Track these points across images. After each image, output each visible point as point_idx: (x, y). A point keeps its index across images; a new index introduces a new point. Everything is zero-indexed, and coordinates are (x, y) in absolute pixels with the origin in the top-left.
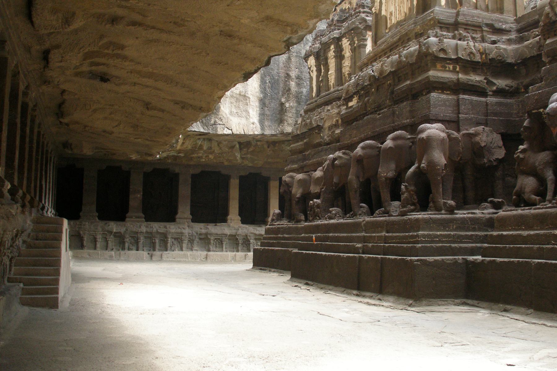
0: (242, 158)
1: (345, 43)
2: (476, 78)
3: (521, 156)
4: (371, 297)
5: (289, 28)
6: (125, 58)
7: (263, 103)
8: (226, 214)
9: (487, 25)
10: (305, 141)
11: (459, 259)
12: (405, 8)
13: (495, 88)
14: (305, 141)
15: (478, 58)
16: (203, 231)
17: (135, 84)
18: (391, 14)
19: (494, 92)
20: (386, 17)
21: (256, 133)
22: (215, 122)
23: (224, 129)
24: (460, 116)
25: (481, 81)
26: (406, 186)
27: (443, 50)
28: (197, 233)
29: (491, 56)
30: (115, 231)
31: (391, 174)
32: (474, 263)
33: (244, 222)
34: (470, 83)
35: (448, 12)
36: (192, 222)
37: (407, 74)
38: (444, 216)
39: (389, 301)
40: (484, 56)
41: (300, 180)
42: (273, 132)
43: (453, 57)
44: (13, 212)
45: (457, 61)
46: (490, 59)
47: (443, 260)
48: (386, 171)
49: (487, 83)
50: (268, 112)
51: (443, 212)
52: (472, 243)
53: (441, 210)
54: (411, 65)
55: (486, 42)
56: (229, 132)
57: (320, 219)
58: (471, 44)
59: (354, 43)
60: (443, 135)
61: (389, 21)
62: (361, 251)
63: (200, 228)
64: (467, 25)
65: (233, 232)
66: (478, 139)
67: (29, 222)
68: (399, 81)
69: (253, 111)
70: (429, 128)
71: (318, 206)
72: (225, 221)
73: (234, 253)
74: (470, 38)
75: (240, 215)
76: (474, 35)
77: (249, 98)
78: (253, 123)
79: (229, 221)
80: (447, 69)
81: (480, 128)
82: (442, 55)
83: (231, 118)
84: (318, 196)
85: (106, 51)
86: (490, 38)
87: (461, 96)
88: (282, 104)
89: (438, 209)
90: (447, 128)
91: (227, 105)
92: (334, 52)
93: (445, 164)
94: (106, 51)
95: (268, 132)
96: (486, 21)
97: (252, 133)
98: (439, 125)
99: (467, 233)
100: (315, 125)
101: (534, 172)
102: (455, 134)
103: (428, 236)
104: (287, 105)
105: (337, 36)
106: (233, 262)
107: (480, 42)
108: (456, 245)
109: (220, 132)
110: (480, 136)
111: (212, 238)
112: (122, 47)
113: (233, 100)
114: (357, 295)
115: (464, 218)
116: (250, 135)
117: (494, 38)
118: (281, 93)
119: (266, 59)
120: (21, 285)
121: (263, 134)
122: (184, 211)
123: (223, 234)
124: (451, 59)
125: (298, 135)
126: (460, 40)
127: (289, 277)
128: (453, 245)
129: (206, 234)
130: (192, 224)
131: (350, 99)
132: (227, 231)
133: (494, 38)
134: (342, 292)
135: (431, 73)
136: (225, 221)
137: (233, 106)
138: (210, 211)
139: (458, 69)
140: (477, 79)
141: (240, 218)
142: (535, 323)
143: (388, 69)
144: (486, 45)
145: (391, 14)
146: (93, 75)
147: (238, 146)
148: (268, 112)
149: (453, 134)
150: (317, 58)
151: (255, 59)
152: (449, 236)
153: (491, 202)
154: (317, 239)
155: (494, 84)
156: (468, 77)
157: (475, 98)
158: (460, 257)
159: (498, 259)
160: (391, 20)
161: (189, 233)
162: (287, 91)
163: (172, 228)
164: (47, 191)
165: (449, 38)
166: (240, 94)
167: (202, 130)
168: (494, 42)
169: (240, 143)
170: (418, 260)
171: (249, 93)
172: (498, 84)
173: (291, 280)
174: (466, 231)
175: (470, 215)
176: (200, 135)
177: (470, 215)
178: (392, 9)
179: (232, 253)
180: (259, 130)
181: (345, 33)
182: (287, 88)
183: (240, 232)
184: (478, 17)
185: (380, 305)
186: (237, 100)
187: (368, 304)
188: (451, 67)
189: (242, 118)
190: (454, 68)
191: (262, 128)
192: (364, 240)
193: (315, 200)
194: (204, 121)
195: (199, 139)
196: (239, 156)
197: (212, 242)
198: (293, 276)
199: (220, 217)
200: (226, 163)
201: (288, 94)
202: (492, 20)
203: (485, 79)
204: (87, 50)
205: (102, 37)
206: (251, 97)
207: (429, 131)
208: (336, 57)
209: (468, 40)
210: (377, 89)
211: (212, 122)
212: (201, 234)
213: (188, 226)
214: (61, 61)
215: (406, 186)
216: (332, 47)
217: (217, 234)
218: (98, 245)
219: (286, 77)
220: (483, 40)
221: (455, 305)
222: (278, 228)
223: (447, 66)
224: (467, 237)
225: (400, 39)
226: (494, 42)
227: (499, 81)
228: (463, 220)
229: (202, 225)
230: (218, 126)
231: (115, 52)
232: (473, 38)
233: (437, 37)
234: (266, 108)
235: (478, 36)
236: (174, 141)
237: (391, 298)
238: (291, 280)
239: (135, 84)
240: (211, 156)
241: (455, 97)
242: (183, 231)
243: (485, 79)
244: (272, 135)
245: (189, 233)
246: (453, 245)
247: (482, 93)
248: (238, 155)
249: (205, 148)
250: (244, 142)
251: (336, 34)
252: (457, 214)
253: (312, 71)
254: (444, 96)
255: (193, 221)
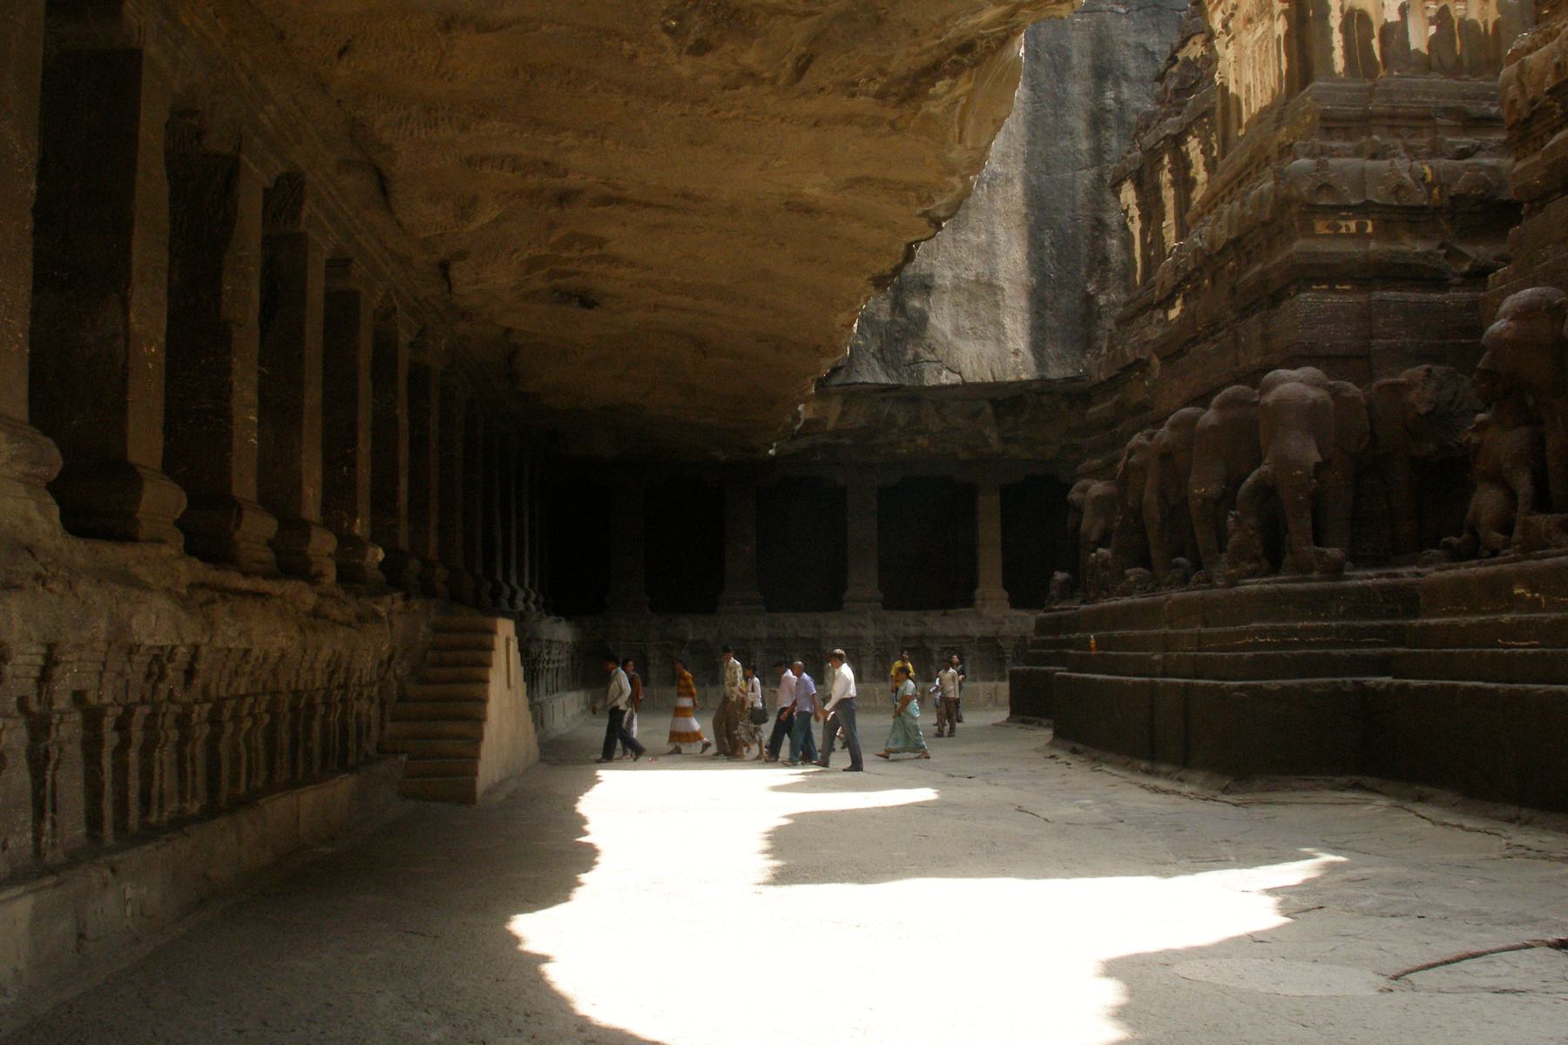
0: (1005, 440)
1: (1193, 146)
2: (1414, 246)
3: (1475, 439)
4: (1168, 776)
5: (911, 194)
6: (615, 260)
7: (1039, 302)
8: (973, 584)
9: (1448, 111)
10: (1116, 397)
11: (1344, 683)
12: (1271, 80)
13: (1466, 268)
14: (1116, 397)
15: (1419, 198)
16: (913, 630)
17: (656, 307)
18: (1248, 87)
19: (1466, 275)
20: (1238, 100)
21: (1024, 377)
22: (917, 355)
23: (940, 373)
24: (1374, 342)
25: (1430, 253)
26: (1236, 517)
27: (1326, 187)
28: (896, 637)
29: (1454, 190)
30: (691, 637)
31: (1213, 489)
32: (1374, 691)
33: (1015, 604)
34: (1398, 261)
35: (1349, 90)
36: (886, 607)
37: (1259, 245)
38: (1315, 585)
39: (1191, 782)
40: (1436, 191)
41: (1097, 498)
42: (1070, 373)
43: (1353, 202)
44: (382, 609)
45: (1365, 209)
46: (1451, 198)
47: (1303, 685)
48: (1202, 487)
49: (1447, 256)
50: (1052, 322)
51: (1315, 575)
52: (1386, 645)
53: (1311, 571)
54: (1263, 224)
55: (1443, 155)
56: (956, 379)
57: (1110, 595)
58: (1402, 164)
59: (1212, 148)
60: (1313, 394)
61: (1244, 108)
62: (1159, 670)
63: (906, 623)
64: (1392, 117)
65: (989, 630)
66: (1412, 396)
67: (423, 628)
68: (1249, 262)
69: (1015, 321)
70: (1283, 381)
71: (1105, 564)
72: (969, 602)
73: (993, 684)
74: (1400, 150)
75: (1005, 587)
76: (1412, 142)
77: (1002, 289)
78: (1016, 353)
79: (979, 602)
80: (1343, 231)
81: (1420, 370)
82: (1324, 201)
83: (959, 343)
84: (1104, 541)
85: (566, 254)
86: (1452, 145)
87: (1377, 295)
88: (1089, 299)
89: (1303, 570)
90: (1329, 375)
91: (946, 311)
92: (1170, 171)
93: (1317, 465)
94: (566, 254)
95: (1055, 373)
96: (1443, 103)
97: (1011, 378)
98: (1308, 371)
99: (1374, 623)
100: (1131, 361)
101: (1498, 479)
102: (1352, 389)
103: (1274, 632)
104: (1102, 299)
105: (1174, 132)
106: (990, 706)
107: (1431, 155)
108: (1342, 651)
109: (930, 380)
110: (1418, 390)
111: (936, 647)
112: (601, 242)
113: (961, 298)
114: (1148, 772)
115: (1365, 586)
116: (1011, 383)
117: (1465, 141)
118: (1083, 271)
119: (903, 248)
120: (404, 758)
121: (1042, 380)
122: (864, 581)
123: (966, 637)
124: (1348, 208)
125: (1102, 383)
126: (1373, 157)
127: (1047, 734)
128: (1335, 652)
129: (921, 638)
130: (885, 613)
131: (1168, 303)
132: (974, 628)
133: (1465, 141)
134: (1124, 766)
135: (1299, 245)
136: (969, 602)
137: (962, 314)
138: (928, 576)
139: (1369, 230)
140: (1419, 250)
141: (1006, 594)
142: (1445, 824)
143: (1223, 235)
144: (1443, 163)
145: (1248, 87)
146: (565, 296)
147: (989, 410)
148: (1052, 322)
149: (1347, 390)
150: (1139, 187)
151: (879, 250)
152: (1326, 631)
153: (1448, 546)
154: (1100, 643)
155: (1465, 257)
156: (1393, 248)
157: (1412, 296)
158: (1349, 680)
159: (1412, 681)
160: (1248, 103)
161: (876, 638)
162: (1100, 263)
163: (833, 625)
164: (514, 551)
165: (1348, 156)
166: (977, 281)
167: (884, 379)
168: (1463, 154)
169: (995, 403)
170: (1241, 688)
171: (1002, 275)
172: (1474, 256)
173: (1051, 745)
174: (1373, 618)
175: (1384, 580)
176: (884, 391)
177: (1384, 580)
178: (1248, 77)
179: (988, 684)
180: (1033, 368)
181: (1190, 125)
182: (1099, 257)
183: (1007, 629)
184: (1427, 94)
185: (1174, 792)
186: (973, 298)
187: (1156, 790)
188: (1353, 225)
189: (988, 343)
190: (1361, 227)
191: (1041, 363)
192: (1167, 644)
193: (1100, 550)
194: (889, 356)
195: (884, 399)
196: (994, 435)
197: (936, 657)
198: (1057, 734)
199: (956, 591)
200: (963, 455)
201: (1103, 271)
202: (1464, 97)
203: (1441, 246)
204: (526, 256)
205: (552, 226)
206: (1006, 285)
207: (1281, 387)
208: (1174, 184)
209: (1394, 156)
210: (1213, 281)
211: (909, 356)
212: (906, 639)
213: (875, 621)
214: (477, 282)
215: (1236, 517)
216: (1166, 159)
217: (946, 637)
218: (653, 675)
219: (1094, 228)
220: (1435, 152)
221: (1334, 789)
222: (1060, 617)
223: (1343, 223)
224: (1371, 631)
225: (1251, 158)
226: (1463, 154)
227: (1481, 248)
228: (1365, 593)
229: (910, 615)
230: (926, 367)
231: (586, 253)
232: (1412, 152)
233: (1313, 157)
234: (1048, 312)
235: (1422, 141)
236: (789, 420)
237: (1199, 777)
238: (1051, 745)
239: (656, 307)
240: (922, 441)
241: (1363, 298)
242: (862, 632)
243: (1441, 246)
244: (1073, 380)
245: (876, 638)
246: (1335, 652)
247: (1438, 281)
248: (993, 437)
249: (901, 420)
250: (1004, 399)
251: (1170, 126)
252: (1349, 578)
253: (1132, 219)
254: (1333, 299)
255: (888, 606)
